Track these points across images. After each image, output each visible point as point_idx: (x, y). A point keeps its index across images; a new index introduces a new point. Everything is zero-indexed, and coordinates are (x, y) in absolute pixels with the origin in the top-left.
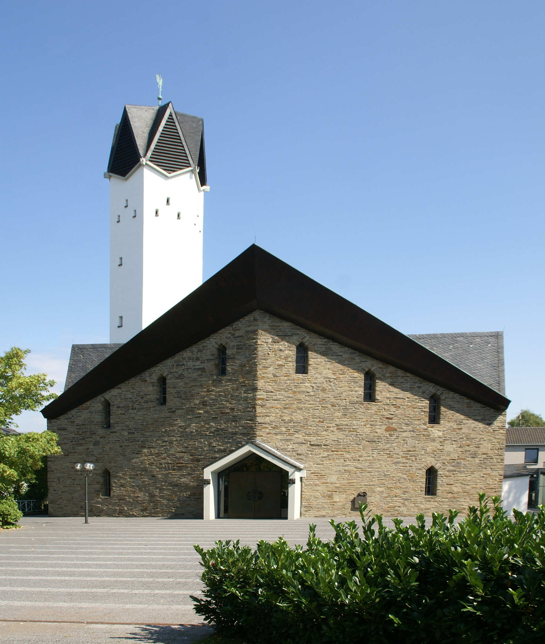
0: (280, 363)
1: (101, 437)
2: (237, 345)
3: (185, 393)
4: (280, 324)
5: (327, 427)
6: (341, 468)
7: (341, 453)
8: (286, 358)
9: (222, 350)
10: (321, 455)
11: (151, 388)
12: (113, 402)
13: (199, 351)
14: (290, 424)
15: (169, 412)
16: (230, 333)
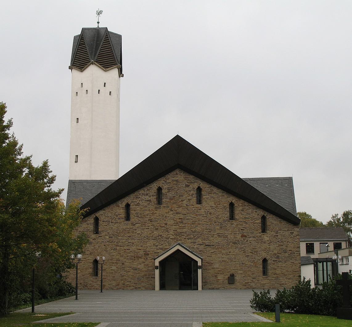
0: (189, 198)
1: (93, 240)
2: (168, 188)
3: (141, 214)
4: (189, 176)
5: (213, 235)
6: (220, 259)
7: (220, 250)
8: (192, 195)
9: (160, 189)
10: (210, 252)
11: (122, 211)
12: (101, 218)
13: (148, 190)
14: (195, 233)
15: (132, 225)
16: (164, 181)
